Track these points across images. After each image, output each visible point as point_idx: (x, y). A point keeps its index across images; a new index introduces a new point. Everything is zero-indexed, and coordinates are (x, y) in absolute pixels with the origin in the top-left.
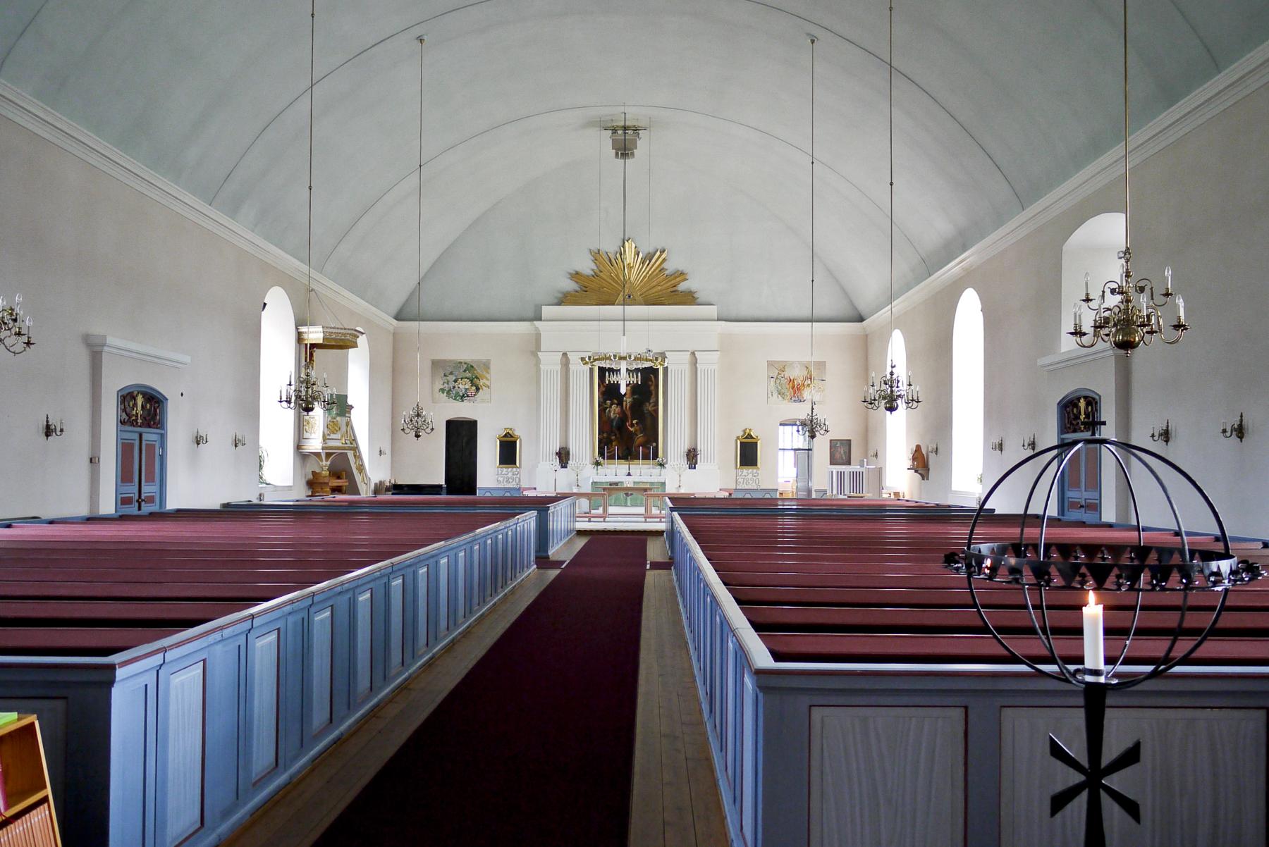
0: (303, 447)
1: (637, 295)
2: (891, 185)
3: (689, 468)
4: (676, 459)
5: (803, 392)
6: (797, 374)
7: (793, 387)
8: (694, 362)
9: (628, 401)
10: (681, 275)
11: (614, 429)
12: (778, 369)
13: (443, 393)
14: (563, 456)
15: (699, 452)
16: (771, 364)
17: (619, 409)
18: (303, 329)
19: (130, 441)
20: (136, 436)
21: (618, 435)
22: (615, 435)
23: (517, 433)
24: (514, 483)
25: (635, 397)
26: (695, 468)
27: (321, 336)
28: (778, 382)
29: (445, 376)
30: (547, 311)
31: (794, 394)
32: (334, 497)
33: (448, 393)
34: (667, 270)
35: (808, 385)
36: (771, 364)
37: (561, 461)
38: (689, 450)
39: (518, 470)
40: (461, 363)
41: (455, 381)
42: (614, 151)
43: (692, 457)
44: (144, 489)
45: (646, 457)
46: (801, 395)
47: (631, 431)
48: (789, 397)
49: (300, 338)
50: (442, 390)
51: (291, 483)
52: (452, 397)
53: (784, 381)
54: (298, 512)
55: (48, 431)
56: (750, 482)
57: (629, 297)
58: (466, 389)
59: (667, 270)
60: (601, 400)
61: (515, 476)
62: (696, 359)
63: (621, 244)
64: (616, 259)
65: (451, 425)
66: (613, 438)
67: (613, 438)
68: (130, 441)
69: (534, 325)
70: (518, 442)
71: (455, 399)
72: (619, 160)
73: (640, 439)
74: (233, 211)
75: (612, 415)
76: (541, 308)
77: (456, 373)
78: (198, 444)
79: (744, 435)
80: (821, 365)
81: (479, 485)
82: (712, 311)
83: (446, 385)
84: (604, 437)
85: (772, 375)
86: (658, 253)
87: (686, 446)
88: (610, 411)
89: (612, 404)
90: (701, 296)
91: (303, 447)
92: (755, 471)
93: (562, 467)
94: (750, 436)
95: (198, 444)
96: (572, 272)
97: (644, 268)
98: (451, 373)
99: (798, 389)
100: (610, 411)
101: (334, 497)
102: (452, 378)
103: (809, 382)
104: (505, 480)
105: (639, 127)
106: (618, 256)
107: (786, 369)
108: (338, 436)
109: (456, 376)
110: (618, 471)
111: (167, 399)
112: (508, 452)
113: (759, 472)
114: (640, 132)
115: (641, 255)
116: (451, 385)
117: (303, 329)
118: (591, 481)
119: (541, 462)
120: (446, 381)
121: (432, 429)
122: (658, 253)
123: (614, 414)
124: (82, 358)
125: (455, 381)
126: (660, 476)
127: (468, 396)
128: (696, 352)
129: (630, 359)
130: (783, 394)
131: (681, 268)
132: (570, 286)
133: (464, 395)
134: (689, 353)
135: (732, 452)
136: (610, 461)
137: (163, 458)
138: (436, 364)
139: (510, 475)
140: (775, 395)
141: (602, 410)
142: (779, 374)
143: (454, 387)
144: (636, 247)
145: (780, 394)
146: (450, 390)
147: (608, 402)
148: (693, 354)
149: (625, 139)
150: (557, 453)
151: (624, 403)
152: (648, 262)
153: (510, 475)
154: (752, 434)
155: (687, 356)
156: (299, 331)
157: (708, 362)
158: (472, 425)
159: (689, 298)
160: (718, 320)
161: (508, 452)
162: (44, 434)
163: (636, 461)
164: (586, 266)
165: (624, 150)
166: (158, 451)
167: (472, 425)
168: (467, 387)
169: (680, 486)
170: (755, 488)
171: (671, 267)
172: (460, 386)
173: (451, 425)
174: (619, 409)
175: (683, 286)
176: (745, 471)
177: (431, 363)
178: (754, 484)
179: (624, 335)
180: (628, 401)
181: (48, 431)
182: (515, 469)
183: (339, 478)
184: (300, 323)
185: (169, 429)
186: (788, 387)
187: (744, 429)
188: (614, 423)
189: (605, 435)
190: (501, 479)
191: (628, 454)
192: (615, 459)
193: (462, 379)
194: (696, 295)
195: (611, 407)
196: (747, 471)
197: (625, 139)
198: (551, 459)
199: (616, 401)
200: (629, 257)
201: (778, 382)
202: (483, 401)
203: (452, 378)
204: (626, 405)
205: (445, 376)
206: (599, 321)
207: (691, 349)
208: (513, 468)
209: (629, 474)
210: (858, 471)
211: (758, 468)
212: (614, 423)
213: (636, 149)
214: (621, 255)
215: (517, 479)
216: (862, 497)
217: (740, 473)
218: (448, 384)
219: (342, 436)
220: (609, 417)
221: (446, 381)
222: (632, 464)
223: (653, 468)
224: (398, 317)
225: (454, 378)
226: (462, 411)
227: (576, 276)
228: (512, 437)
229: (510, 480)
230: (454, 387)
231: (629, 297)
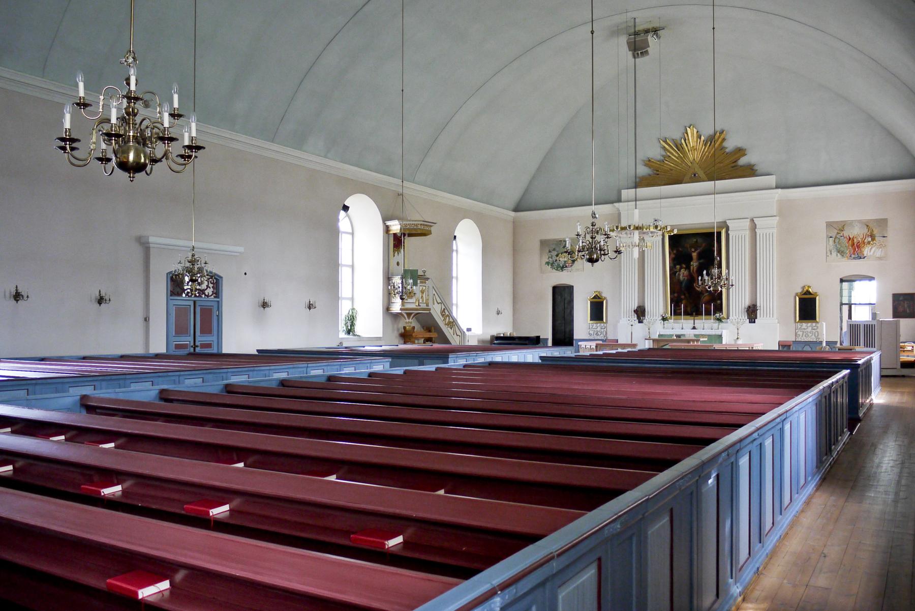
0: (391, 309)
1: (701, 173)
2: (592, 33)
3: (750, 322)
4: (734, 314)
5: (863, 249)
6: (857, 232)
7: (853, 244)
8: (753, 227)
9: (695, 265)
10: (740, 152)
11: (683, 289)
12: (837, 229)
13: (548, 265)
14: (640, 313)
15: (758, 308)
16: (829, 225)
17: (686, 273)
18: (388, 223)
19: (209, 307)
20: (192, 304)
21: (687, 295)
22: (684, 295)
23: (604, 295)
24: (602, 335)
25: (701, 261)
26: (754, 322)
27: (399, 227)
28: (837, 241)
29: (550, 252)
30: (626, 193)
31: (854, 251)
32: (432, 345)
33: (552, 265)
34: (727, 148)
35: (869, 243)
36: (829, 225)
37: (639, 318)
38: (749, 307)
39: (605, 325)
40: (561, 241)
41: (557, 256)
42: (631, 52)
43: (752, 313)
44: (198, 338)
45: (708, 313)
46: (862, 252)
47: (698, 291)
48: (848, 255)
49: (387, 229)
50: (548, 263)
51: (381, 335)
52: (554, 268)
53: (845, 241)
54: (394, 356)
55: (101, 300)
56: (807, 332)
57: (695, 175)
58: (565, 262)
59: (727, 148)
60: (672, 265)
61: (602, 330)
62: (756, 225)
63: (684, 131)
64: (681, 144)
65: (555, 289)
66: (683, 297)
67: (683, 297)
68: (209, 307)
69: (615, 206)
70: (817, 298)
71: (556, 270)
72: (640, 59)
73: (705, 298)
74: (299, 141)
75: (681, 278)
76: (621, 192)
77: (557, 249)
78: (310, 309)
79: (802, 292)
80: (883, 223)
81: (575, 337)
82: (771, 180)
83: (551, 259)
84: (674, 296)
85: (830, 235)
86: (686, 135)
87: (747, 302)
88: (679, 274)
89: (681, 268)
90: (760, 168)
91: (391, 309)
92: (814, 324)
93: (639, 322)
94: (808, 293)
95: (310, 309)
96: (645, 159)
97: (707, 148)
98: (554, 250)
99: (858, 247)
100: (679, 274)
101: (432, 345)
102: (555, 253)
103: (870, 239)
104: (595, 333)
105: (657, 27)
106: (683, 141)
107: (845, 229)
108: (413, 300)
109: (557, 252)
110: (705, 325)
111: (222, 278)
112: (597, 310)
113: (818, 325)
114: (659, 32)
115: (703, 138)
116: (554, 258)
117: (388, 223)
118: (658, 334)
119: (623, 319)
120: (550, 256)
121: (28, 297)
122: (686, 135)
123: (683, 276)
124: (137, 252)
125: (557, 256)
126: (718, 329)
127: (566, 267)
128: (754, 219)
129: (630, 228)
130: (842, 252)
131: (739, 145)
132: (643, 171)
133: (563, 266)
134: (749, 220)
135: (792, 307)
136: (708, 317)
137: (219, 318)
138: (544, 243)
139: (599, 329)
140: (834, 253)
141: (673, 274)
142: (838, 233)
143: (556, 260)
144: (697, 132)
145: (839, 252)
146: (553, 263)
147: (678, 267)
148: (752, 220)
149: (635, 41)
150: (634, 311)
151: (692, 267)
152: (709, 142)
153: (599, 329)
154: (810, 290)
155: (747, 223)
156: (387, 224)
157: (768, 227)
158: (569, 289)
159: (750, 171)
160: (777, 187)
161: (597, 310)
162: (97, 303)
163: (700, 317)
164: (655, 152)
165: (638, 48)
166: (215, 313)
167: (569, 289)
168: (566, 260)
169: (738, 338)
170: (815, 340)
171: (731, 144)
172: (561, 259)
173: (555, 289)
174: (686, 273)
175: (743, 161)
176: (804, 325)
177: (539, 244)
178: (813, 337)
179: (636, 208)
180: (695, 265)
181: (101, 300)
182: (602, 325)
183: (430, 331)
184: (385, 219)
185: (224, 297)
186: (847, 245)
187: (802, 285)
188: (683, 285)
189: (676, 295)
190: (592, 332)
191: (694, 311)
192: (681, 315)
193: (562, 253)
194: (755, 168)
195: (680, 271)
196: (807, 326)
197: (635, 41)
198: (628, 316)
199: (684, 266)
200: (692, 142)
201: (837, 241)
202: (578, 270)
203: (555, 253)
204: (693, 268)
205: (550, 252)
206: (661, 199)
207: (751, 215)
208: (601, 323)
209: (694, 328)
210: (871, 324)
211: (817, 322)
212: (683, 285)
213: (649, 47)
214: (685, 141)
215: (604, 333)
216: (851, 349)
217: (799, 327)
218: (552, 258)
219: (416, 300)
220: (679, 280)
221: (550, 256)
222: (697, 319)
223: (714, 323)
224: (516, 210)
225: (556, 253)
226: (563, 278)
227: (648, 163)
228: (599, 298)
229: (599, 333)
230: (556, 260)
231: (695, 175)
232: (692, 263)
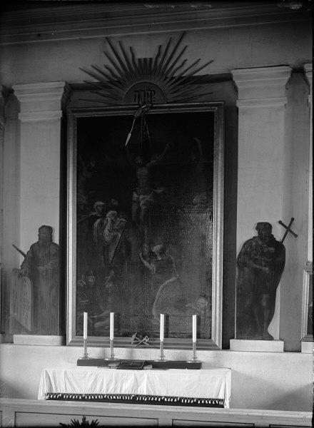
88: (101, 224)
151: (135, 207)
195: (104, 216)
232: (135, 195)
